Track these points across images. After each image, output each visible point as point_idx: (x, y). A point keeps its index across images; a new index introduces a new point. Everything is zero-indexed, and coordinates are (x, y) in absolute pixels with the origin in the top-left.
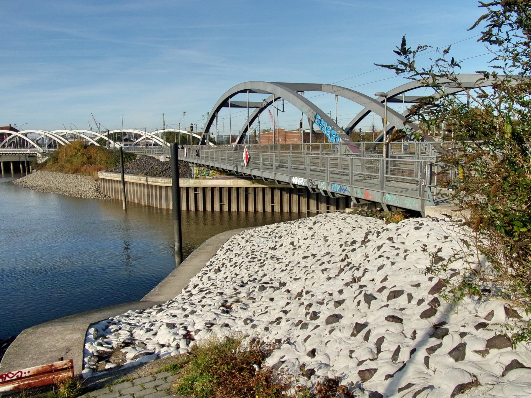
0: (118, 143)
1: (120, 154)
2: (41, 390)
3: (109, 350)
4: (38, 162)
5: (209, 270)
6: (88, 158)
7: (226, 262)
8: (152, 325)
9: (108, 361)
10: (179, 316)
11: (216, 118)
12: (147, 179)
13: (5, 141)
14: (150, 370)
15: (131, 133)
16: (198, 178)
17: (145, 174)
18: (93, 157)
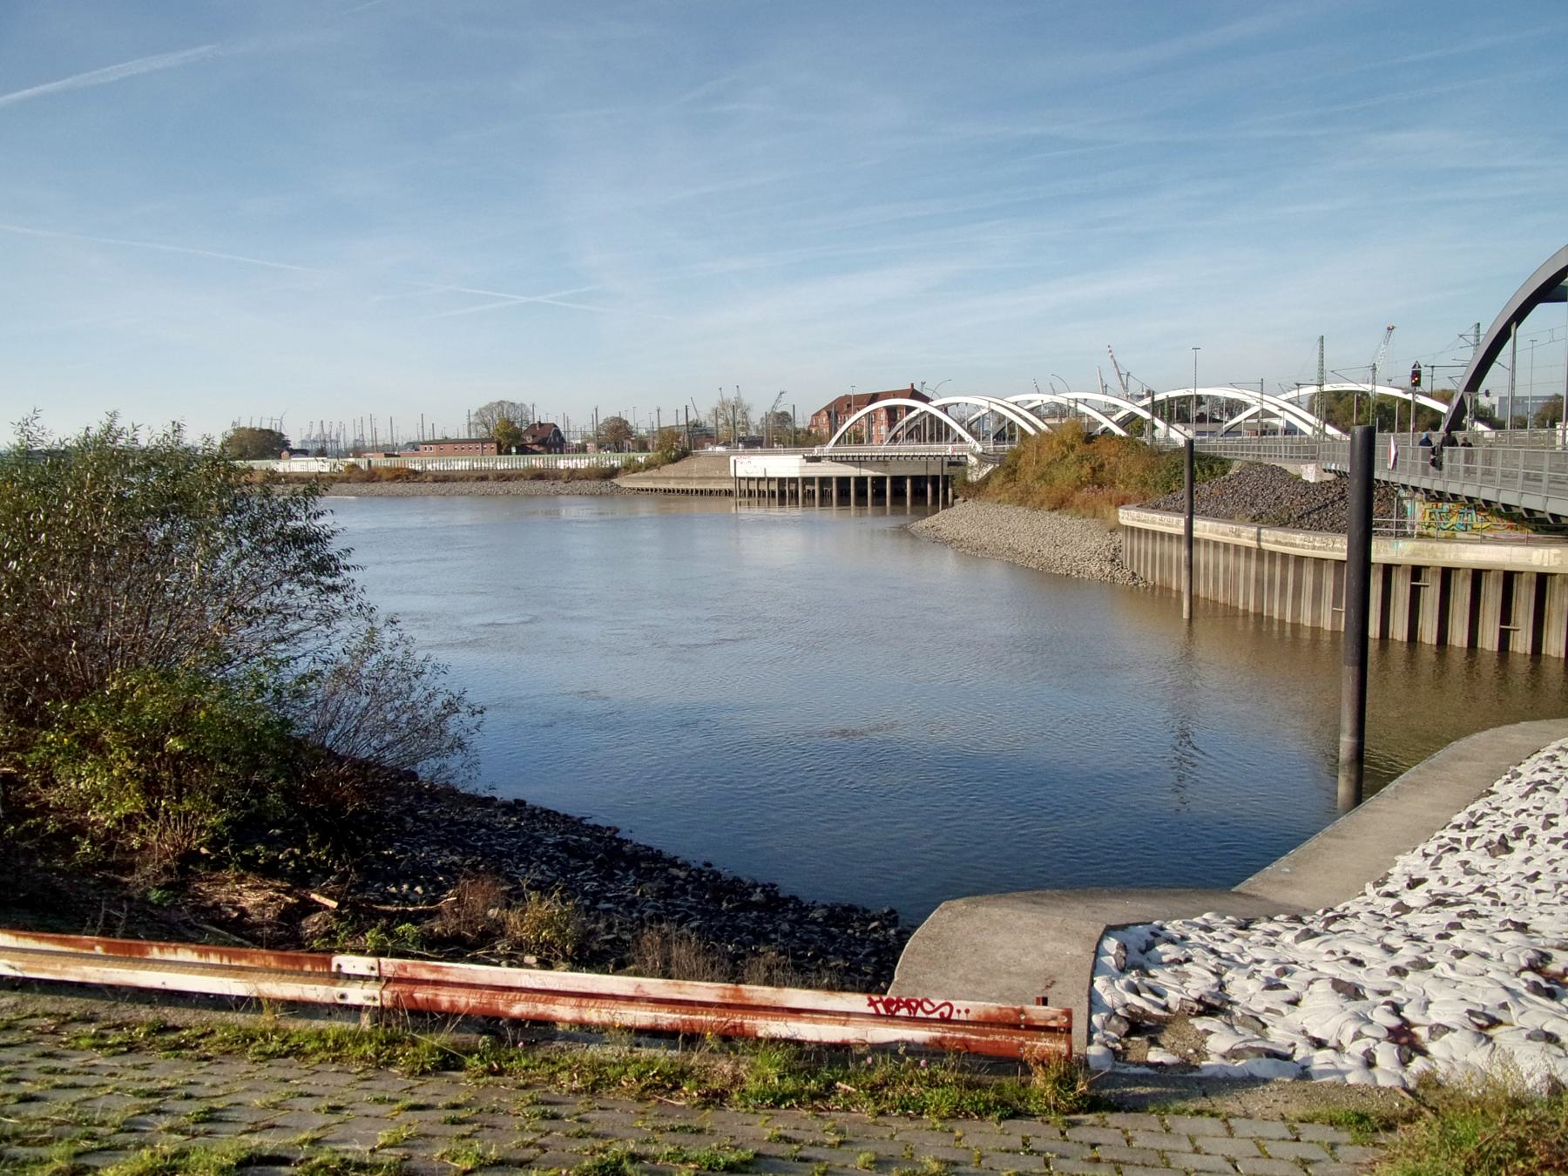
0: (1177, 426)
1: (1186, 460)
2: (990, 1066)
3: (1156, 1012)
4: (969, 478)
5: (1464, 840)
6: (1093, 469)
7: (1534, 825)
8: (1284, 972)
9: (1154, 1042)
10: (1372, 966)
11: (1511, 341)
12: (1259, 534)
13: (899, 425)
14: (1278, 1105)
15: (1215, 399)
16: (1429, 536)
17: (1254, 519)
18: (1107, 467)
